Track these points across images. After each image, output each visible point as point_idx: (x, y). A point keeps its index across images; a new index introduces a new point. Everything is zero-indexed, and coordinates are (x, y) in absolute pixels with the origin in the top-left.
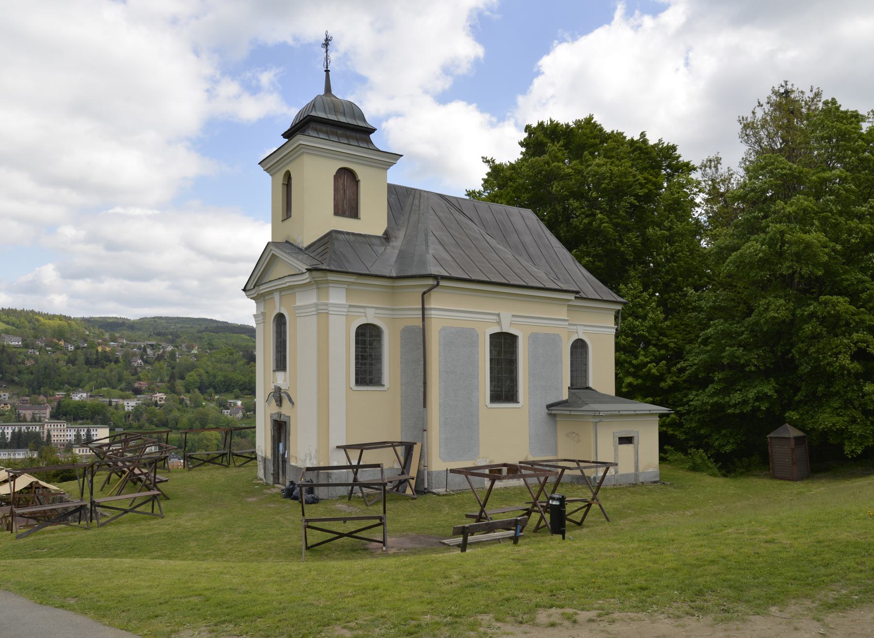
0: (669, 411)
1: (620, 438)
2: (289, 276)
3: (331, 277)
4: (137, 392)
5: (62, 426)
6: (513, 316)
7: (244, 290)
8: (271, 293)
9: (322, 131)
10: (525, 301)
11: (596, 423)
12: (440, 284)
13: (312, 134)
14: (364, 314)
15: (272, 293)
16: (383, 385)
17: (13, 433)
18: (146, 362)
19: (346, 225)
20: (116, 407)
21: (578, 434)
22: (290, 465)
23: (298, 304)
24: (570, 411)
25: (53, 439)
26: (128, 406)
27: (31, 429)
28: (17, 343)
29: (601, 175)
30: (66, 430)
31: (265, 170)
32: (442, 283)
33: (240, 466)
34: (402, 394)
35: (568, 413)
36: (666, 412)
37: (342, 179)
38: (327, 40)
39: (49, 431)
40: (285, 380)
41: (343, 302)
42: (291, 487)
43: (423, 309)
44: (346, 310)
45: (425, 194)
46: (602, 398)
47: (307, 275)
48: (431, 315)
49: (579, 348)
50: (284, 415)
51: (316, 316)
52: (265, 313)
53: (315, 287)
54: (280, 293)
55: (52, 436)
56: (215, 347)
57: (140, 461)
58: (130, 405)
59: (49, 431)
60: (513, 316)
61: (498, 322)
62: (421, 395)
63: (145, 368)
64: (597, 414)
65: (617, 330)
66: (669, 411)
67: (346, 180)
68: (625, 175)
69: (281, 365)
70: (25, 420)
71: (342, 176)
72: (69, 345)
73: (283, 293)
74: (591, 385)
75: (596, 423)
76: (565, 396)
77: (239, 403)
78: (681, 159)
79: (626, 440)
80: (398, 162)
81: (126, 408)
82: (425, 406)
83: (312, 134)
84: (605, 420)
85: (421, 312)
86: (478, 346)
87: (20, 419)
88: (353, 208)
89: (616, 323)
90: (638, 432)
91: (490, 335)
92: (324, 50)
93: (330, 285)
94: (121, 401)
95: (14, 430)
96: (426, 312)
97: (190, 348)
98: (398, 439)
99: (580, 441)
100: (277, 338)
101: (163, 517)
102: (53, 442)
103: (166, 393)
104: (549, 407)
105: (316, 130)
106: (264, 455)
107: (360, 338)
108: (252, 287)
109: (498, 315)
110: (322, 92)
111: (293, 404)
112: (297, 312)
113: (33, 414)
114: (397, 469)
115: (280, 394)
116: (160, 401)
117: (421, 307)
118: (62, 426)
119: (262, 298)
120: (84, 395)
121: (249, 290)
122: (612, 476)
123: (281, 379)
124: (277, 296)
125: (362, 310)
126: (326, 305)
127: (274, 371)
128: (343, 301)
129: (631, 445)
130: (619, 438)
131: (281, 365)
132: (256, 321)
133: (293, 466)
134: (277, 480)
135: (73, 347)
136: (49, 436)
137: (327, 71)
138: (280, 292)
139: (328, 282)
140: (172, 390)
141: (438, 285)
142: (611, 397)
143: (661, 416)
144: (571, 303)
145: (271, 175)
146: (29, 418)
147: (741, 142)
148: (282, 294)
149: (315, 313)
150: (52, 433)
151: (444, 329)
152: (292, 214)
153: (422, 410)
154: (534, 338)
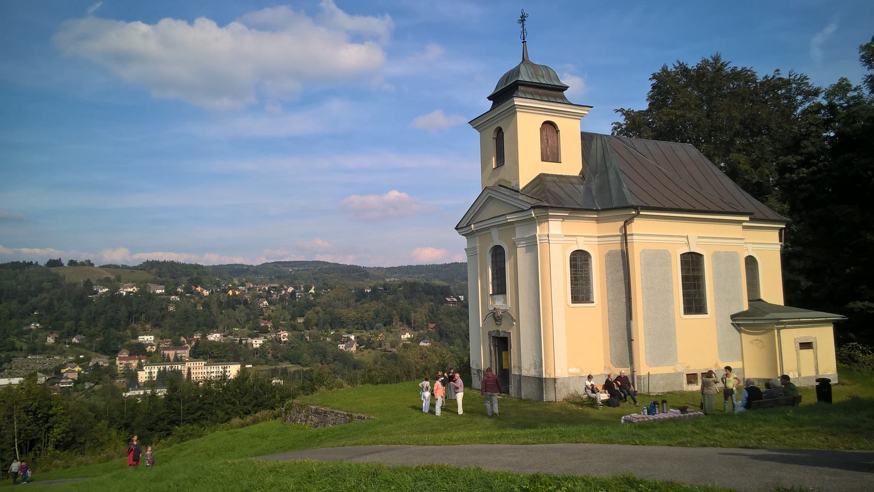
0: (843, 317)
1: (801, 344)
4: (264, 331)
5: (200, 364)
6: (699, 237)
7: (457, 228)
9: (528, 93)
12: (641, 213)
13: (520, 95)
15: (489, 229)
17: (159, 372)
18: (270, 303)
19: (551, 168)
20: (246, 344)
25: (193, 376)
26: (256, 344)
27: (174, 367)
28: (161, 291)
30: (203, 368)
34: (609, 309)
35: (801, 320)
38: (523, 17)
39: (189, 369)
41: (560, 232)
45: (605, 137)
46: (774, 308)
49: (751, 262)
51: (524, 248)
55: (192, 374)
56: (329, 286)
58: (257, 343)
59: (189, 369)
60: (699, 237)
63: (269, 309)
65: (781, 246)
66: (843, 317)
67: (549, 129)
69: (500, 288)
70: (169, 360)
71: (545, 129)
72: (205, 291)
74: (762, 297)
76: (745, 307)
77: (353, 337)
79: (806, 345)
81: (254, 346)
83: (520, 95)
86: (671, 265)
87: (166, 360)
88: (554, 154)
89: (780, 241)
91: (681, 255)
92: (521, 25)
94: (250, 340)
95: (159, 369)
96: (628, 238)
97: (307, 289)
102: (192, 379)
103: (288, 331)
104: (733, 317)
105: (525, 93)
113: (176, 354)
116: (284, 338)
118: (200, 364)
120: (218, 335)
121: (461, 228)
122: (796, 378)
123: (498, 303)
124: (494, 233)
125: (574, 239)
129: (810, 350)
130: (800, 343)
131: (500, 288)
135: (208, 293)
136: (189, 373)
140: (293, 328)
141: (638, 214)
144: (744, 224)
146: (172, 358)
149: (525, 245)
150: (192, 371)
151: (644, 251)
154: (716, 256)
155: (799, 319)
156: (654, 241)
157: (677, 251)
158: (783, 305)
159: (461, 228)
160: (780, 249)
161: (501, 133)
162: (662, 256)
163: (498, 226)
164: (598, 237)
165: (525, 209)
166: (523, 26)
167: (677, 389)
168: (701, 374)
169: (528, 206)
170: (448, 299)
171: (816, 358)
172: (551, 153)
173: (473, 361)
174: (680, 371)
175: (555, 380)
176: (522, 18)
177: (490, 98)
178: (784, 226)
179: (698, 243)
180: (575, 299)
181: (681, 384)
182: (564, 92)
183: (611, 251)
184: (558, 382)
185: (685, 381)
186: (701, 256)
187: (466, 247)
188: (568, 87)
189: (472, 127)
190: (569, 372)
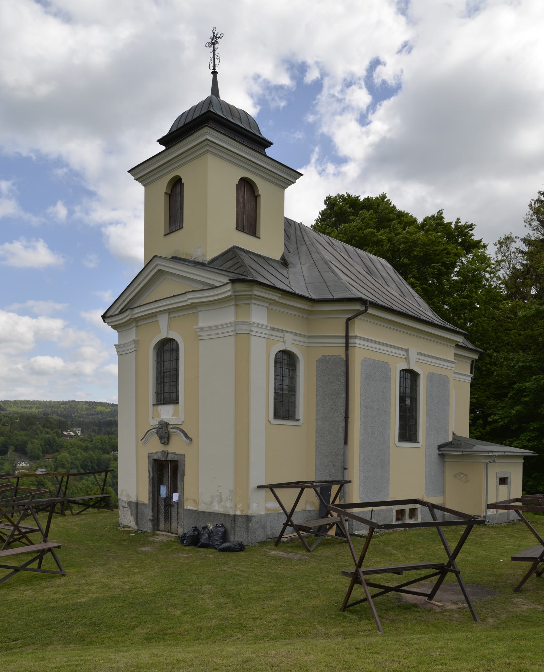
0: (533, 453)
2: (193, 291)
3: (257, 291)
8: (154, 315)
10: (421, 338)
11: (487, 463)
12: (368, 311)
14: (282, 340)
15: (156, 316)
16: (298, 420)
21: (466, 475)
22: (184, 509)
23: (201, 324)
24: (463, 452)
29: (411, 242)
31: (136, 180)
32: (370, 311)
33: (78, 514)
36: (531, 454)
37: (242, 190)
40: (175, 414)
41: (264, 322)
42: (196, 533)
43: (347, 337)
44: (267, 332)
47: (229, 287)
48: (355, 343)
50: (174, 453)
51: (233, 337)
52: (138, 340)
53: (233, 303)
54: (169, 315)
57: (11, 508)
60: (419, 354)
61: (406, 358)
62: (341, 431)
64: (491, 454)
68: (434, 243)
73: (172, 316)
75: (487, 463)
78: (473, 237)
80: (297, 181)
82: (346, 442)
84: (497, 461)
85: (344, 341)
86: (390, 382)
89: (471, 373)
90: (511, 473)
92: (211, 49)
93: (253, 301)
96: (350, 341)
98: (312, 478)
99: (468, 481)
100: (157, 368)
101: (64, 575)
104: (440, 447)
106: (134, 500)
107: (278, 365)
108: (117, 312)
109: (407, 351)
111: (191, 440)
112: (199, 334)
114: (310, 511)
115: (168, 430)
117: (344, 334)
119: (134, 324)
122: (494, 515)
124: (163, 320)
125: (280, 334)
126: (249, 324)
127: (154, 405)
128: (264, 322)
132: (117, 352)
133: (189, 510)
134: (156, 527)
137: (214, 73)
138: (170, 313)
139: (250, 297)
142: (467, 438)
143: (526, 458)
145: (144, 185)
147: (525, 226)
148: (171, 316)
149: (232, 333)
151: (365, 360)
152: (184, 226)
153: (342, 447)
154: (431, 376)
157: (397, 366)
158: (468, 437)
159: (111, 316)
161: (178, 188)
163: (170, 311)
165: (217, 284)
166: (214, 50)
168: (408, 510)
169: (222, 280)
170: (65, 433)
173: (122, 491)
175: (248, 518)
176: (212, 39)
179: (294, 342)
180: (277, 416)
182: (266, 150)
183: (325, 356)
184: (254, 520)
187: (117, 343)
188: (272, 144)
189: (133, 178)
190: (266, 508)
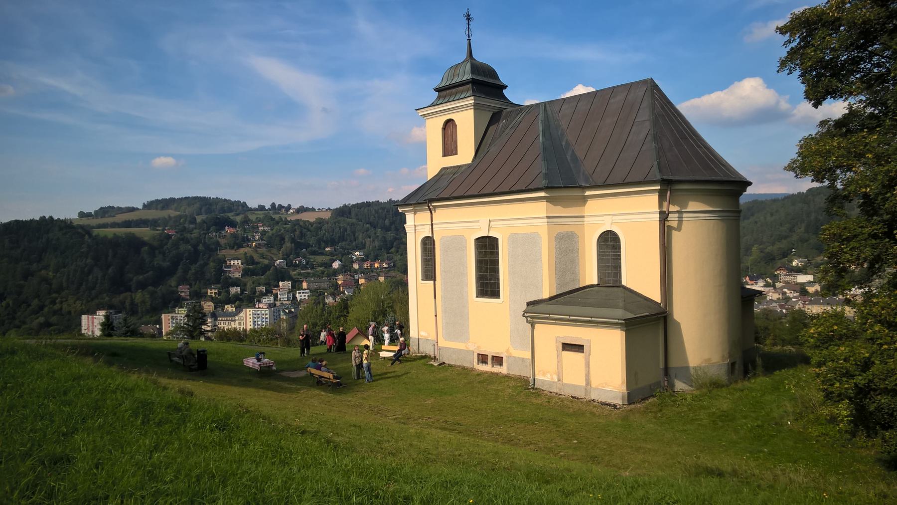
6: (478, 221)
19: (452, 161)
60: (478, 221)
85: (414, 229)
110: (464, 56)
117: (430, 223)
129: (580, 354)
155: (549, 314)
156: (530, 225)
160: (658, 219)
162: (457, 242)
164: (548, 217)
167: (467, 365)
171: (588, 365)
172: (450, 148)
174: (471, 349)
177: (436, 90)
178: (659, 188)
181: (472, 362)
185: (476, 360)
186: (496, 240)
